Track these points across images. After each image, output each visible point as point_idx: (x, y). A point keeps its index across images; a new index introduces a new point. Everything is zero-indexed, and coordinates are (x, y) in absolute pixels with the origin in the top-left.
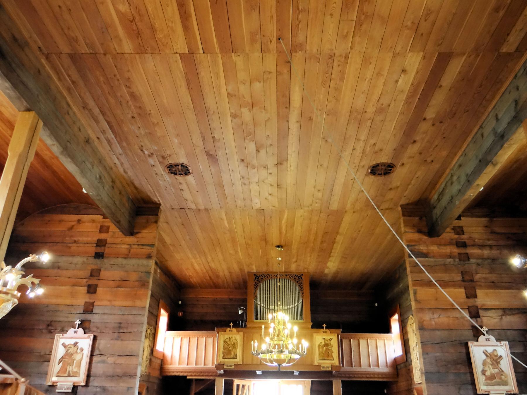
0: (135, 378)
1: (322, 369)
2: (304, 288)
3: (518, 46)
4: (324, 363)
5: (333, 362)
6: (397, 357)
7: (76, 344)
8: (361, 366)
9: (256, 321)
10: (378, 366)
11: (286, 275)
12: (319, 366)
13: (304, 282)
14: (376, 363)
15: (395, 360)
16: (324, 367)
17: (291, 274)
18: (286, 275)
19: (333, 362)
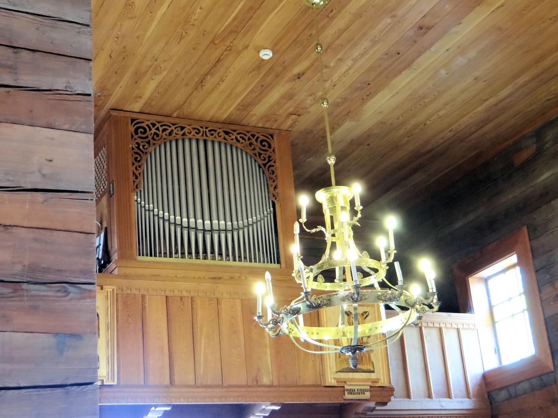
0: (323, 354)
1: (348, 396)
2: (279, 172)
3: (549, 338)
4: (353, 380)
5: (373, 376)
6: (490, 372)
7: (130, 323)
8: (408, 396)
9: (141, 258)
10: (449, 396)
11: (227, 133)
12: (340, 388)
13: (277, 156)
14: (442, 388)
15: (487, 380)
16: (351, 392)
17: (239, 129)
18: (227, 133)
19: (373, 376)
